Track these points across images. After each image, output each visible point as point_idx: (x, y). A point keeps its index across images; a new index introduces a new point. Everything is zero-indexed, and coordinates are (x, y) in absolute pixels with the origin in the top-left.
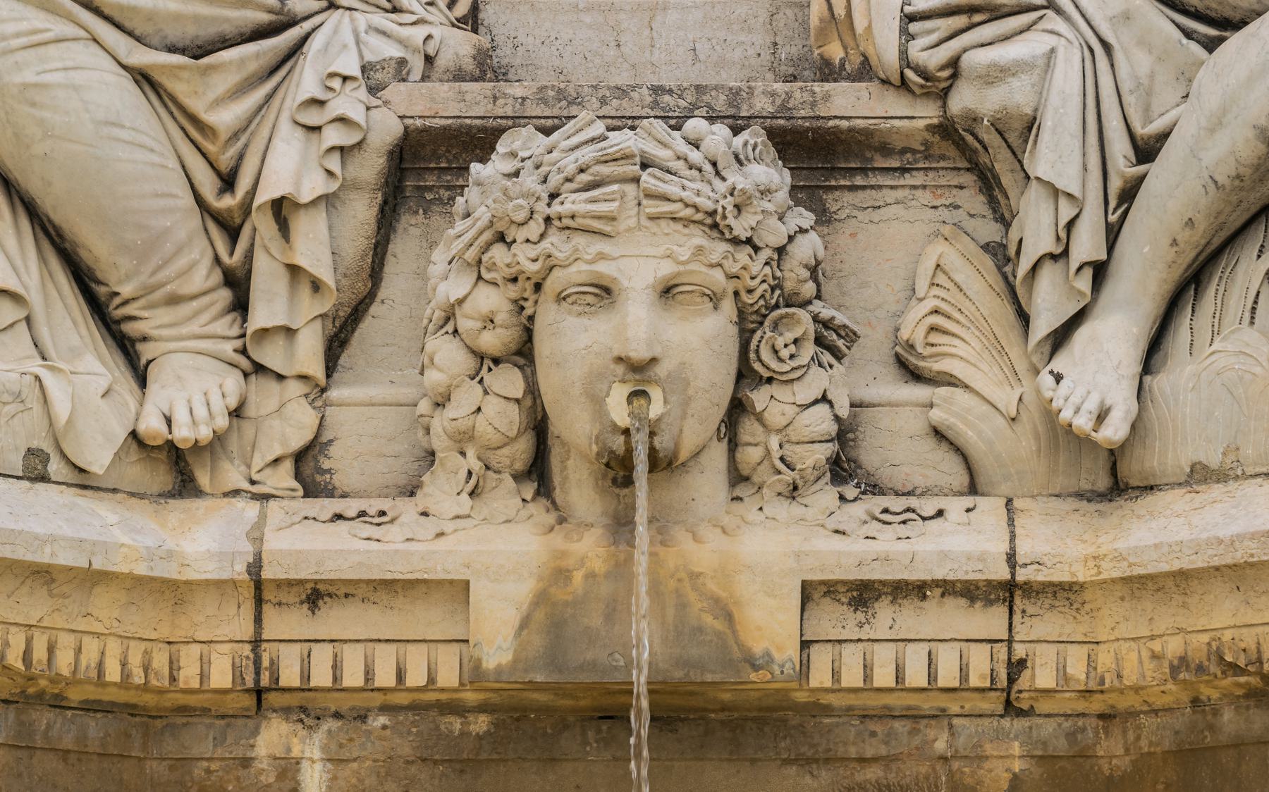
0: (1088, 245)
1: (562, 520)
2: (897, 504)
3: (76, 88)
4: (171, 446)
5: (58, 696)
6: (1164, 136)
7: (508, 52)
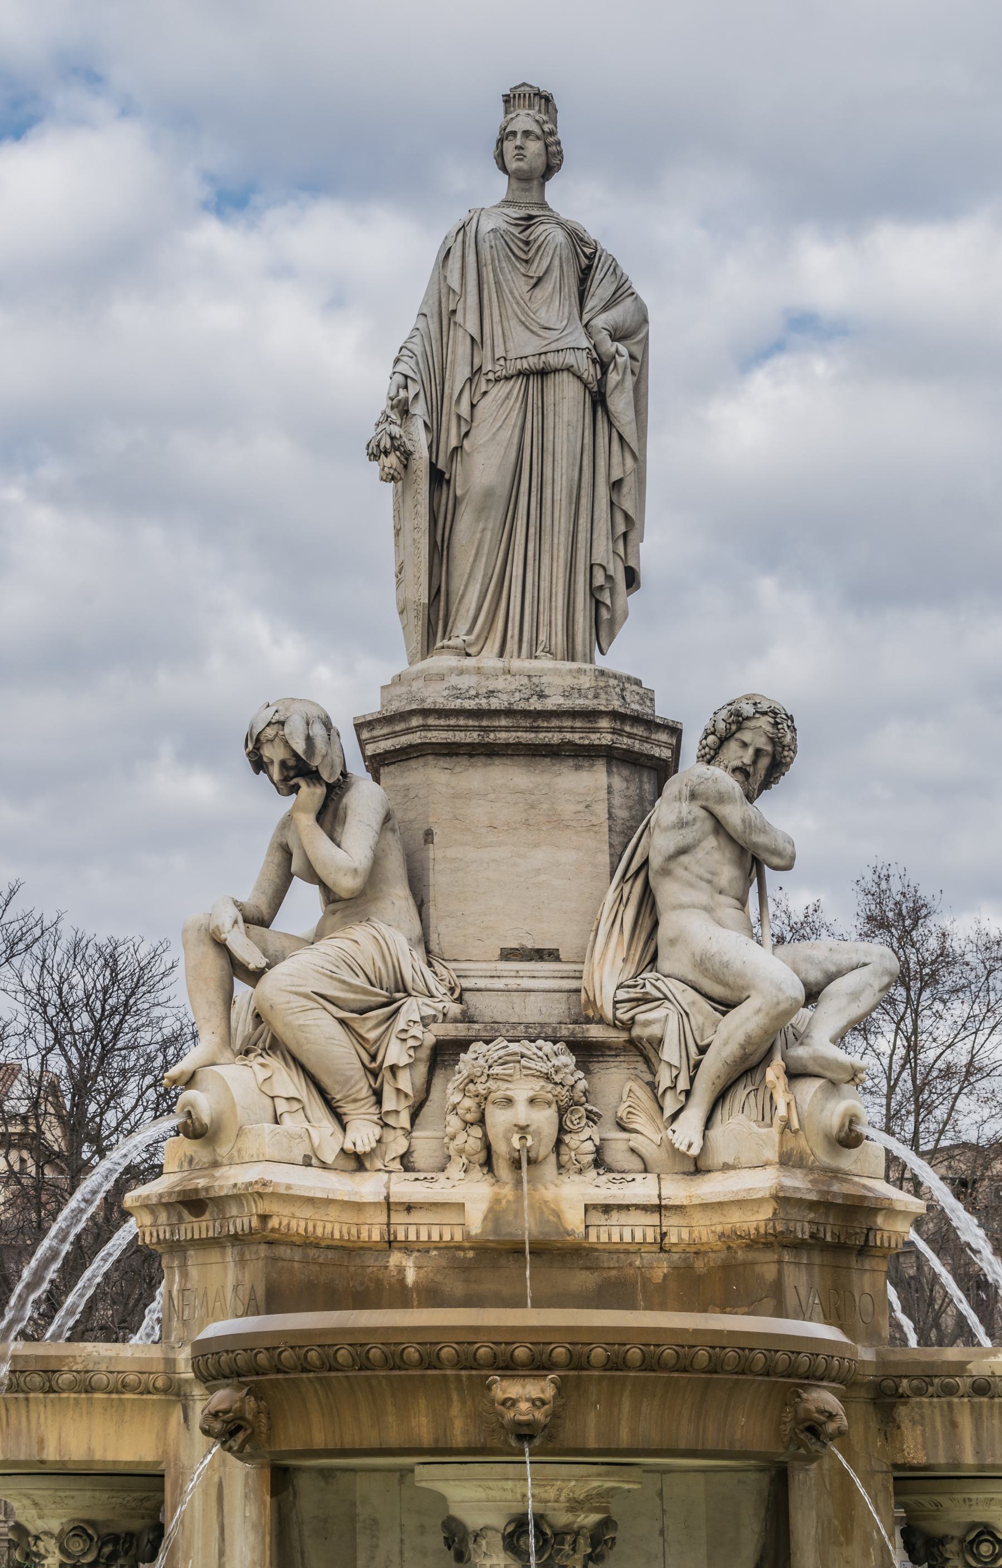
0: (683, 1084)
1: (497, 1181)
2: (618, 1176)
3: (318, 1026)
4: (355, 1153)
6: (708, 1046)
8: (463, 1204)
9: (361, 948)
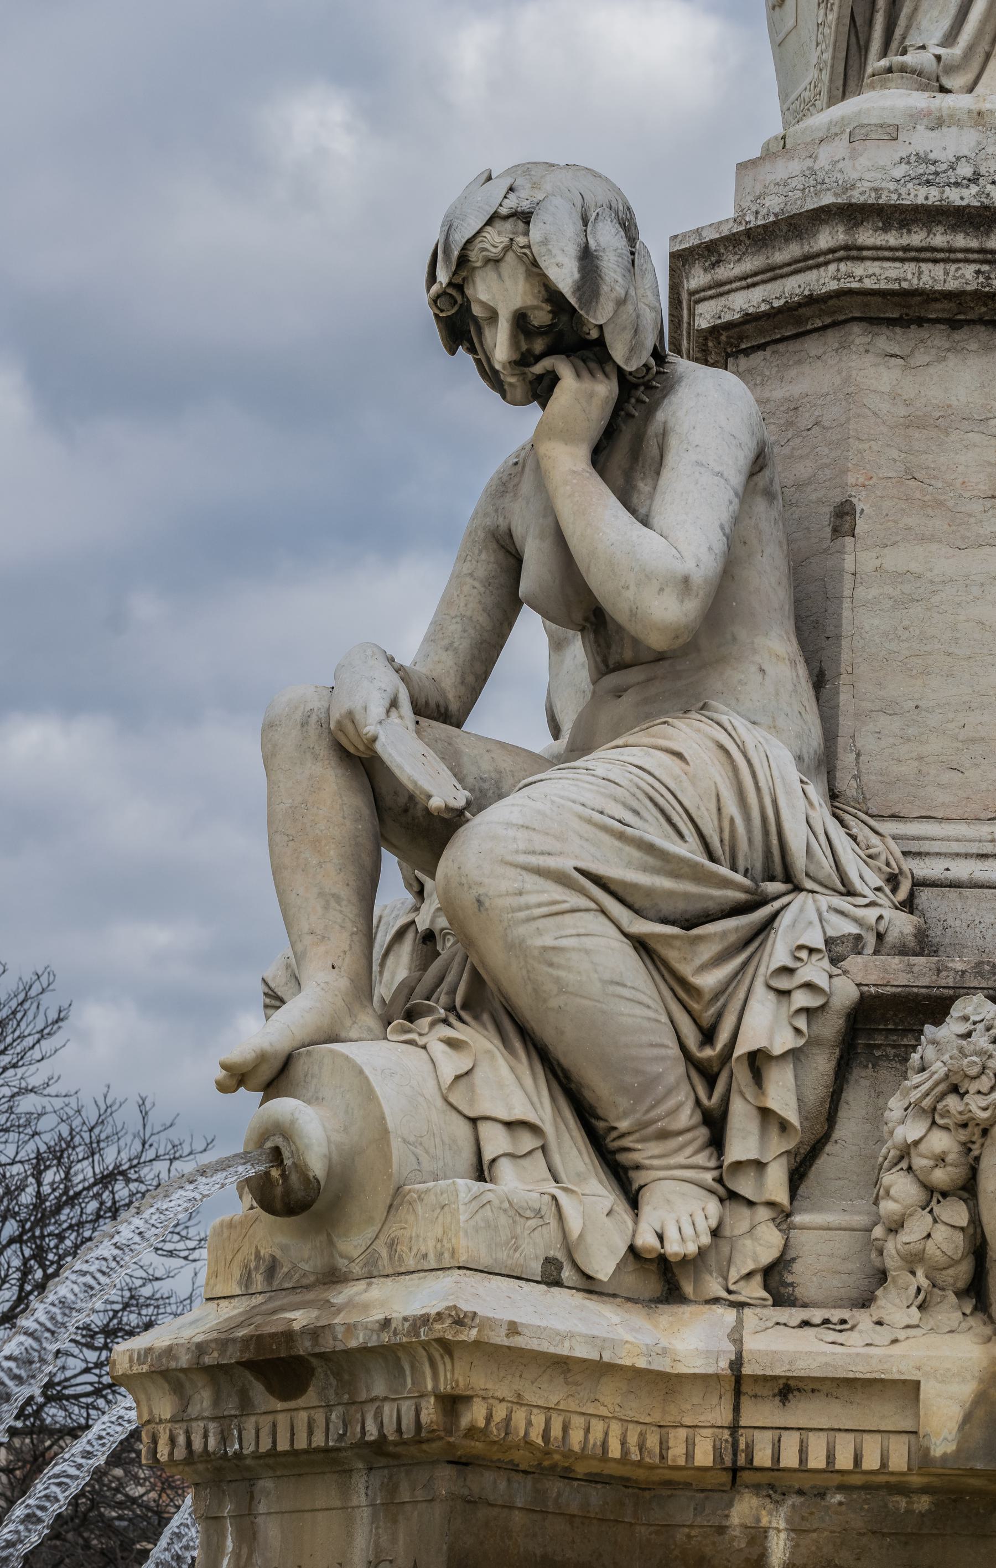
3: (587, 952)
5: (568, 1469)
7: (939, 933)
8: (918, 1383)
9: (690, 769)
